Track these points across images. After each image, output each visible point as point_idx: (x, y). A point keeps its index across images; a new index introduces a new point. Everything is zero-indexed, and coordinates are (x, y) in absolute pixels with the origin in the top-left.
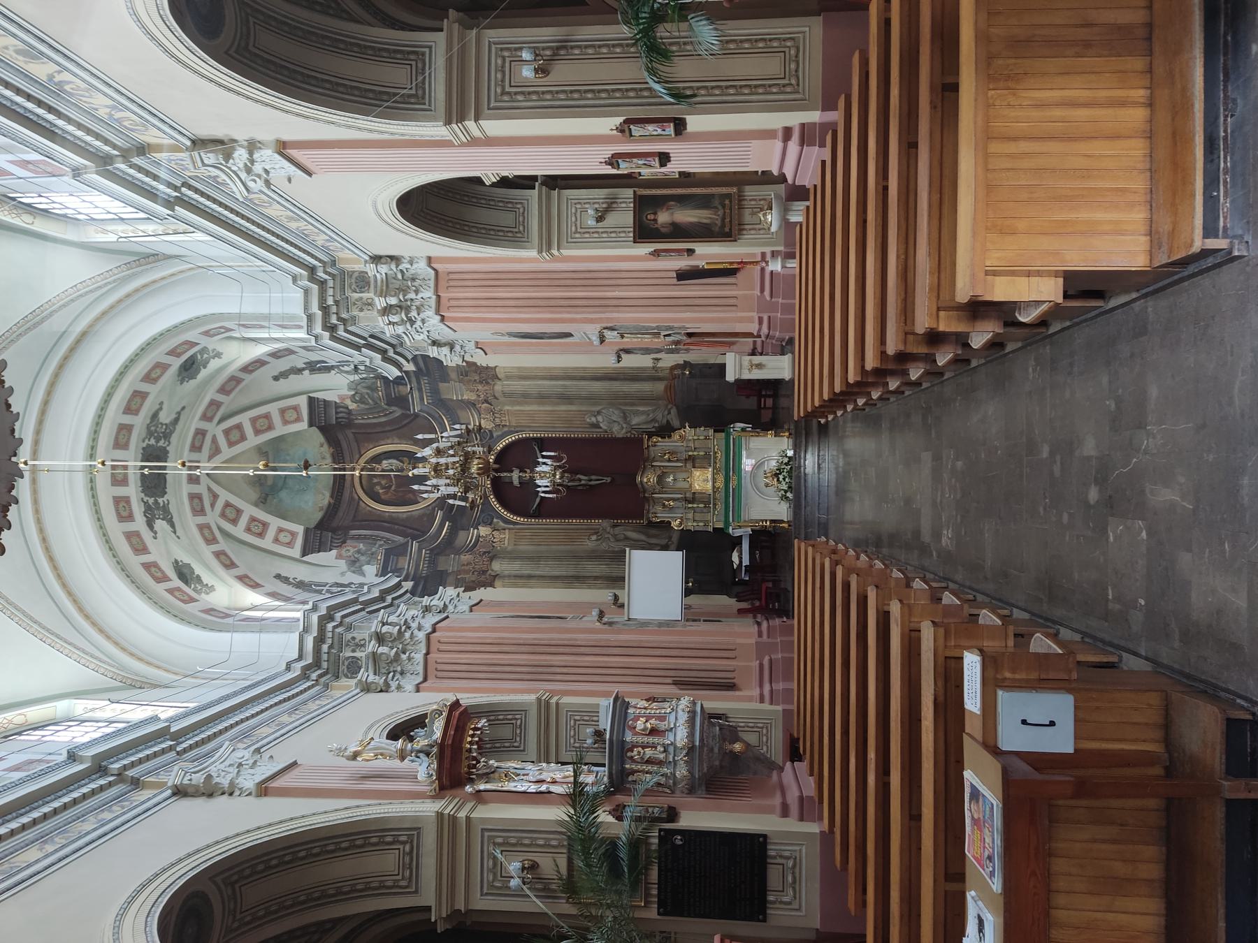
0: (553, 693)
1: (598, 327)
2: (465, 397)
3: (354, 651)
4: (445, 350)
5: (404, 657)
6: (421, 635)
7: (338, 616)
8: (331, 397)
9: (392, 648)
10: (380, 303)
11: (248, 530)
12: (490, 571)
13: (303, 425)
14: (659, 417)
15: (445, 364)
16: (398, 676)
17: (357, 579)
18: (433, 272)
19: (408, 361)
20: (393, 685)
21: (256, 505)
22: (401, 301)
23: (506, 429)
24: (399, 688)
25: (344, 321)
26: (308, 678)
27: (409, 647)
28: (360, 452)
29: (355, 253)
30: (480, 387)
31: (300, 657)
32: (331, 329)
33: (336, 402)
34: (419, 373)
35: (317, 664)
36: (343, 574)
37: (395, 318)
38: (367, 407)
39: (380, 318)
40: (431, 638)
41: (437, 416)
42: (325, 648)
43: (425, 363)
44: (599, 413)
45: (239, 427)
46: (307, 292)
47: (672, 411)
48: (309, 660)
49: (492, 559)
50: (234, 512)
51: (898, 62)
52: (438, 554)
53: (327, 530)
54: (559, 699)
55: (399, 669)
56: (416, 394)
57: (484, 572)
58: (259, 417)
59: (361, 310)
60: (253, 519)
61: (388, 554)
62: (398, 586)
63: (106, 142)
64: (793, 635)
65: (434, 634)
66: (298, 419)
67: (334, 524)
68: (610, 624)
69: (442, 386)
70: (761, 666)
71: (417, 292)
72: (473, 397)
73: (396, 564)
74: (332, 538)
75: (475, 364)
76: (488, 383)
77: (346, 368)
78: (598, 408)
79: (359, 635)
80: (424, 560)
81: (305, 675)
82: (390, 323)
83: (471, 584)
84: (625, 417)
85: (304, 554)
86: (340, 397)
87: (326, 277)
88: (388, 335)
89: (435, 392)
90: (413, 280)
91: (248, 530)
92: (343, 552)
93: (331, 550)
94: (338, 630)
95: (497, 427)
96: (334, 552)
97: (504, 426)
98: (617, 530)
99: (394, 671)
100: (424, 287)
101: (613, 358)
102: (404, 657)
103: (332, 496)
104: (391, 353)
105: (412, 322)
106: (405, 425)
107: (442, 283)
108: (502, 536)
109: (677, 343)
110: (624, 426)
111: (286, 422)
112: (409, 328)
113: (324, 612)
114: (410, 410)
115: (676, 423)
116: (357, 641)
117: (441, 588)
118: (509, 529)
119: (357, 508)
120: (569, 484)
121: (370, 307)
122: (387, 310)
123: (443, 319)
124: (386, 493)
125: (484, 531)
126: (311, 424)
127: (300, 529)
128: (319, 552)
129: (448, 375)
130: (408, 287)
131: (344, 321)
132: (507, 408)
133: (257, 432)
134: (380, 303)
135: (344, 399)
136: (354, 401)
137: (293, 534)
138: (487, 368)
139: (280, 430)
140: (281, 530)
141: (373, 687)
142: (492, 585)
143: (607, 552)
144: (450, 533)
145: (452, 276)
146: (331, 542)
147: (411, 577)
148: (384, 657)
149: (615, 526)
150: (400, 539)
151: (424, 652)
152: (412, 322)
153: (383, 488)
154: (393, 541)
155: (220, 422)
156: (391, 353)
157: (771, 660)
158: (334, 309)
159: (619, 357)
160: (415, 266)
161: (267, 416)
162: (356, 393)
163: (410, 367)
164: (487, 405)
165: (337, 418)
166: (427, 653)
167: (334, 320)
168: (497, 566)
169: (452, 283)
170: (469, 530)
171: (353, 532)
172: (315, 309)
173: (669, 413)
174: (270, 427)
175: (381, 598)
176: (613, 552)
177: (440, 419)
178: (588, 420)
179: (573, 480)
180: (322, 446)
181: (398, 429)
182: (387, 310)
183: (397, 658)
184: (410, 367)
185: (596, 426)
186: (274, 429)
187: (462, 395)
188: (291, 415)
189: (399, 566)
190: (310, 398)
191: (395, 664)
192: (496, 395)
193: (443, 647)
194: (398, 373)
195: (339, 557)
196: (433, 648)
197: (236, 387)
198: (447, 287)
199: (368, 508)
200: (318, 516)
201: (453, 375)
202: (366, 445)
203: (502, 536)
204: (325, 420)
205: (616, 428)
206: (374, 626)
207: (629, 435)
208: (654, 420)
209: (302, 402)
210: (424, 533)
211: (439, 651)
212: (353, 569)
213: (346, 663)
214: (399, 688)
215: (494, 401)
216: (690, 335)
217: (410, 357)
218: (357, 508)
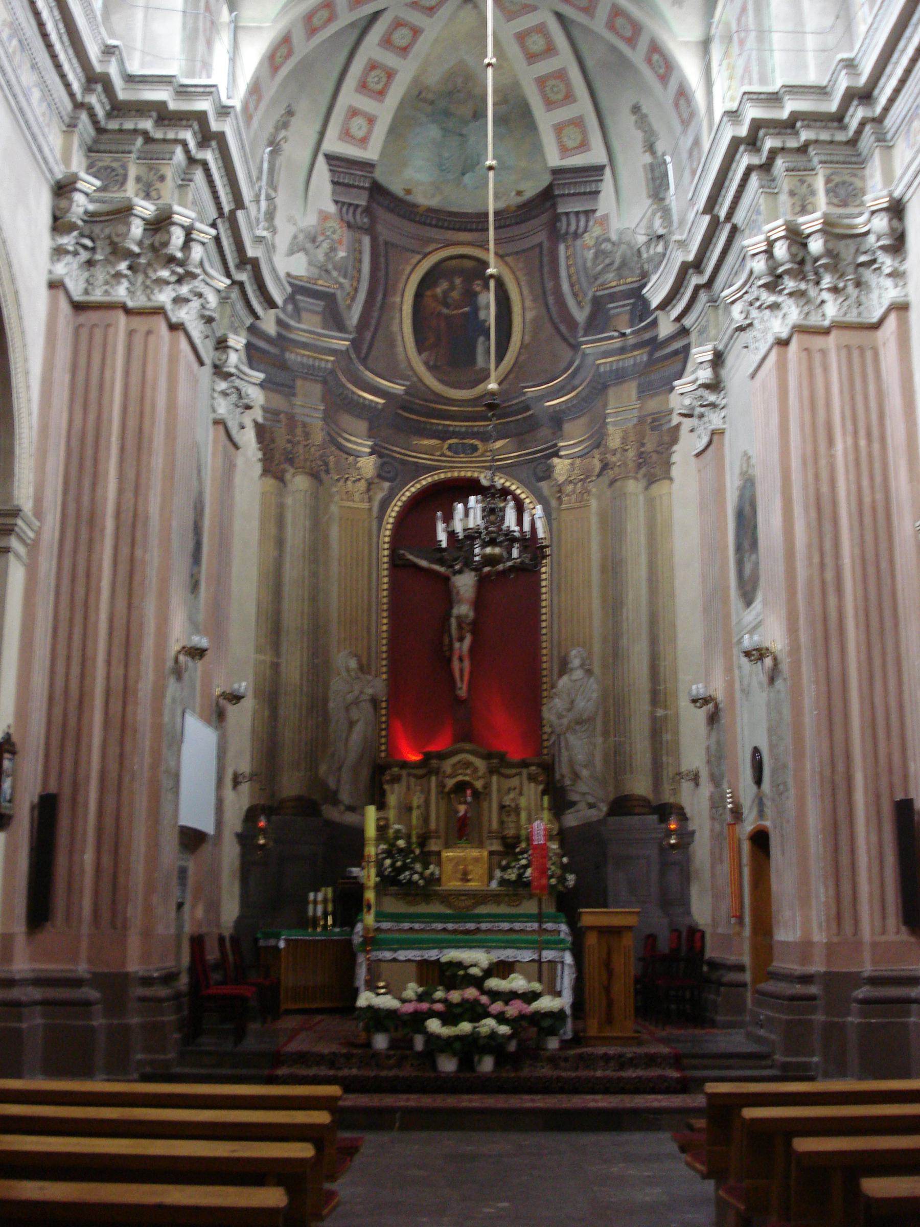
0: (33, 547)
1: (720, 695)
2: (611, 429)
3: (138, 179)
4: (705, 375)
5: (123, 266)
6: (164, 297)
7: (209, 156)
8: (606, 203)
9: (140, 244)
10: (810, 222)
11: (373, 66)
12: (292, 471)
13: (554, 159)
14: (582, 787)
15: (676, 383)
16: (84, 255)
17: (282, 241)
18: (875, 317)
19: (678, 319)
20: (68, 241)
21: (416, 81)
22: (816, 260)
23: (554, 503)
24: (59, 252)
25: (766, 167)
26: (88, 87)
27: (140, 278)
28: (508, 255)
29: (904, 174)
30: (631, 454)
31: (130, 79)
32: (752, 142)
33: (594, 211)
34: (654, 344)
35: (118, 108)
36: (291, 220)
37: (781, 251)
38: (589, 264)
39: (780, 222)
40: (156, 318)
41: (576, 382)
42: (147, 124)
43: (676, 353)
44: (589, 672)
45: (550, 50)
46: (822, 91)
47: (593, 811)
48: (122, 94)
49: (315, 476)
50: (403, 43)
51: (878, 1138)
52: (325, 382)
53: (371, 198)
54: (18, 556)
55: (99, 257)
56: (617, 343)
57: (291, 461)
58: (568, 85)
59: (792, 194)
60: (390, 75)
61: (329, 299)
62: (270, 303)
63: (892, 100)
64: (53, 1070)
65: (164, 328)
66: (565, 151)
67: (383, 214)
68: (178, 672)
69: (631, 389)
70: (77, 983)
71: (835, 290)
72: (614, 440)
73: (310, 311)
74: (357, 206)
75: (675, 440)
76: (639, 466)
77: (657, 222)
78: (597, 669)
79: (168, 190)
80: (315, 358)
81: (93, 79)
82: (771, 244)
83: (267, 435)
84: (580, 722)
85: (329, 158)
86: (606, 217)
87: (854, 125)
88: (746, 243)
89: (620, 376)
90: (858, 284)
91: (373, 66)
92: (334, 224)
93: (336, 202)
94: (179, 151)
95: (556, 489)
96: (332, 208)
97: (559, 498)
98: (367, 707)
99: (93, 250)
100: (846, 303)
101: (699, 689)
102: (123, 266)
103: (430, 210)
104: (695, 280)
105: (773, 286)
106: (557, 329)
107: (854, 338)
108: (357, 497)
109: (737, 813)
110: (565, 721)
111: (559, 129)
112: (761, 282)
113: (215, 125)
114: (584, 336)
115: (571, 820)
116: (158, 185)
117: (262, 376)
118: (370, 509)
119: (407, 250)
120: (453, 621)
121: (798, 209)
122: (797, 238)
123: (783, 343)
124: (435, 297)
125: (368, 465)
126: (557, 172)
127: (371, 153)
128: (334, 183)
129: (652, 396)
130: (842, 276)
131: (766, 167)
132: (594, 504)
133: (541, 82)
134: (810, 222)
135: (601, 224)
136: (599, 241)
137: (363, 141)
138: (668, 465)
139: (545, 120)
140: (371, 120)
141: (63, 204)
142: (266, 472)
143: (327, 686)
144: (364, 406)
145: (869, 354)
146: (350, 205)
147: (284, 332)
148: (121, 229)
149: (374, 702)
150: (354, 317)
151: (130, 304)
152: (773, 286)
153: (446, 294)
154: (349, 307)
155: (559, 16)
156: (695, 280)
157: (87, 1003)
158: (792, 143)
159: (706, 701)
160: (889, 283)
161: (569, 97)
162: (614, 244)
163: (666, 328)
164: (597, 470)
165: (567, 214)
166: (128, 311)
167: (769, 143)
168: (300, 483)
169: (856, 354)
170: (370, 437)
171: (366, 241)
172: (791, 106)
173: (591, 806)
174: (550, 104)
175: (244, 261)
176: (325, 700)
177: (569, 387)
178: (574, 652)
179: (460, 627)
180: (519, 193)
181: (551, 318)
182: (797, 238)
183: (117, 251)
184: (666, 328)
185: (564, 667)
186: (548, 111)
187: (615, 424)
188: (572, 138)
189: (304, 315)
190: (600, 169)
191: (108, 250)
192: (618, 484)
193: (138, 339)
194: (655, 303)
195: (324, 217)
196: (141, 324)
197: (622, 37)
198: (848, 347)
199: (408, 269)
200: (396, 187)
201: (653, 405)
202: (521, 265)
203: (357, 497)
204: (563, 195)
205: (558, 703)
206: (183, 214)
207: (547, 729)
208: (576, 776)
209: (596, 155)
210: (364, 361)
211: (131, 333)
212: (301, 237)
213: (115, 165)
214: (59, 252)
215: (605, 480)
216: (760, 840)
217: (687, 322)
218: (407, 250)
